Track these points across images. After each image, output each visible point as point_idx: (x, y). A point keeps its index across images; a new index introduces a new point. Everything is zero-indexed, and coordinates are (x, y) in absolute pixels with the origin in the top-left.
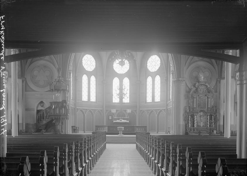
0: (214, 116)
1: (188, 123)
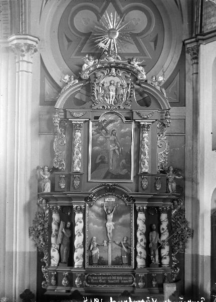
0: (169, 213)
1: (49, 245)
